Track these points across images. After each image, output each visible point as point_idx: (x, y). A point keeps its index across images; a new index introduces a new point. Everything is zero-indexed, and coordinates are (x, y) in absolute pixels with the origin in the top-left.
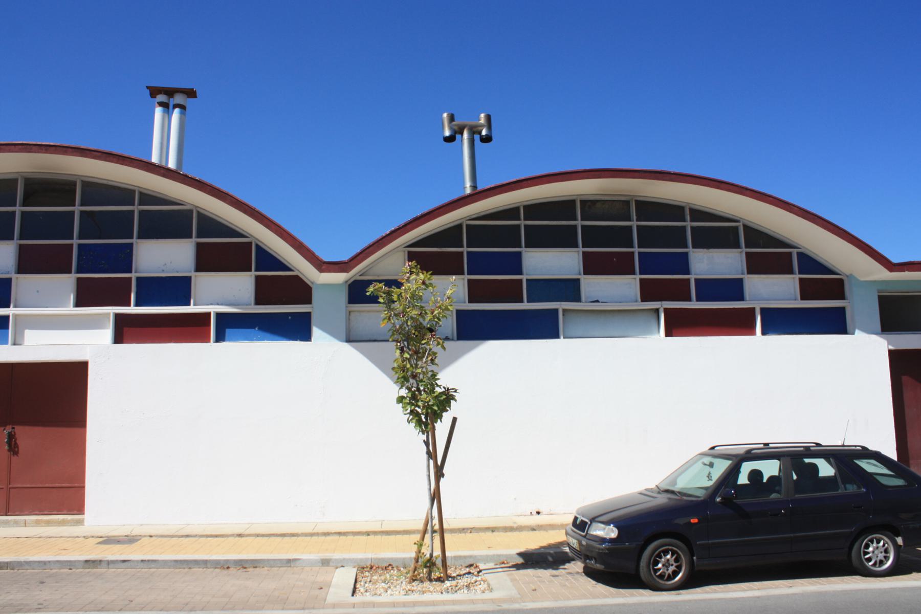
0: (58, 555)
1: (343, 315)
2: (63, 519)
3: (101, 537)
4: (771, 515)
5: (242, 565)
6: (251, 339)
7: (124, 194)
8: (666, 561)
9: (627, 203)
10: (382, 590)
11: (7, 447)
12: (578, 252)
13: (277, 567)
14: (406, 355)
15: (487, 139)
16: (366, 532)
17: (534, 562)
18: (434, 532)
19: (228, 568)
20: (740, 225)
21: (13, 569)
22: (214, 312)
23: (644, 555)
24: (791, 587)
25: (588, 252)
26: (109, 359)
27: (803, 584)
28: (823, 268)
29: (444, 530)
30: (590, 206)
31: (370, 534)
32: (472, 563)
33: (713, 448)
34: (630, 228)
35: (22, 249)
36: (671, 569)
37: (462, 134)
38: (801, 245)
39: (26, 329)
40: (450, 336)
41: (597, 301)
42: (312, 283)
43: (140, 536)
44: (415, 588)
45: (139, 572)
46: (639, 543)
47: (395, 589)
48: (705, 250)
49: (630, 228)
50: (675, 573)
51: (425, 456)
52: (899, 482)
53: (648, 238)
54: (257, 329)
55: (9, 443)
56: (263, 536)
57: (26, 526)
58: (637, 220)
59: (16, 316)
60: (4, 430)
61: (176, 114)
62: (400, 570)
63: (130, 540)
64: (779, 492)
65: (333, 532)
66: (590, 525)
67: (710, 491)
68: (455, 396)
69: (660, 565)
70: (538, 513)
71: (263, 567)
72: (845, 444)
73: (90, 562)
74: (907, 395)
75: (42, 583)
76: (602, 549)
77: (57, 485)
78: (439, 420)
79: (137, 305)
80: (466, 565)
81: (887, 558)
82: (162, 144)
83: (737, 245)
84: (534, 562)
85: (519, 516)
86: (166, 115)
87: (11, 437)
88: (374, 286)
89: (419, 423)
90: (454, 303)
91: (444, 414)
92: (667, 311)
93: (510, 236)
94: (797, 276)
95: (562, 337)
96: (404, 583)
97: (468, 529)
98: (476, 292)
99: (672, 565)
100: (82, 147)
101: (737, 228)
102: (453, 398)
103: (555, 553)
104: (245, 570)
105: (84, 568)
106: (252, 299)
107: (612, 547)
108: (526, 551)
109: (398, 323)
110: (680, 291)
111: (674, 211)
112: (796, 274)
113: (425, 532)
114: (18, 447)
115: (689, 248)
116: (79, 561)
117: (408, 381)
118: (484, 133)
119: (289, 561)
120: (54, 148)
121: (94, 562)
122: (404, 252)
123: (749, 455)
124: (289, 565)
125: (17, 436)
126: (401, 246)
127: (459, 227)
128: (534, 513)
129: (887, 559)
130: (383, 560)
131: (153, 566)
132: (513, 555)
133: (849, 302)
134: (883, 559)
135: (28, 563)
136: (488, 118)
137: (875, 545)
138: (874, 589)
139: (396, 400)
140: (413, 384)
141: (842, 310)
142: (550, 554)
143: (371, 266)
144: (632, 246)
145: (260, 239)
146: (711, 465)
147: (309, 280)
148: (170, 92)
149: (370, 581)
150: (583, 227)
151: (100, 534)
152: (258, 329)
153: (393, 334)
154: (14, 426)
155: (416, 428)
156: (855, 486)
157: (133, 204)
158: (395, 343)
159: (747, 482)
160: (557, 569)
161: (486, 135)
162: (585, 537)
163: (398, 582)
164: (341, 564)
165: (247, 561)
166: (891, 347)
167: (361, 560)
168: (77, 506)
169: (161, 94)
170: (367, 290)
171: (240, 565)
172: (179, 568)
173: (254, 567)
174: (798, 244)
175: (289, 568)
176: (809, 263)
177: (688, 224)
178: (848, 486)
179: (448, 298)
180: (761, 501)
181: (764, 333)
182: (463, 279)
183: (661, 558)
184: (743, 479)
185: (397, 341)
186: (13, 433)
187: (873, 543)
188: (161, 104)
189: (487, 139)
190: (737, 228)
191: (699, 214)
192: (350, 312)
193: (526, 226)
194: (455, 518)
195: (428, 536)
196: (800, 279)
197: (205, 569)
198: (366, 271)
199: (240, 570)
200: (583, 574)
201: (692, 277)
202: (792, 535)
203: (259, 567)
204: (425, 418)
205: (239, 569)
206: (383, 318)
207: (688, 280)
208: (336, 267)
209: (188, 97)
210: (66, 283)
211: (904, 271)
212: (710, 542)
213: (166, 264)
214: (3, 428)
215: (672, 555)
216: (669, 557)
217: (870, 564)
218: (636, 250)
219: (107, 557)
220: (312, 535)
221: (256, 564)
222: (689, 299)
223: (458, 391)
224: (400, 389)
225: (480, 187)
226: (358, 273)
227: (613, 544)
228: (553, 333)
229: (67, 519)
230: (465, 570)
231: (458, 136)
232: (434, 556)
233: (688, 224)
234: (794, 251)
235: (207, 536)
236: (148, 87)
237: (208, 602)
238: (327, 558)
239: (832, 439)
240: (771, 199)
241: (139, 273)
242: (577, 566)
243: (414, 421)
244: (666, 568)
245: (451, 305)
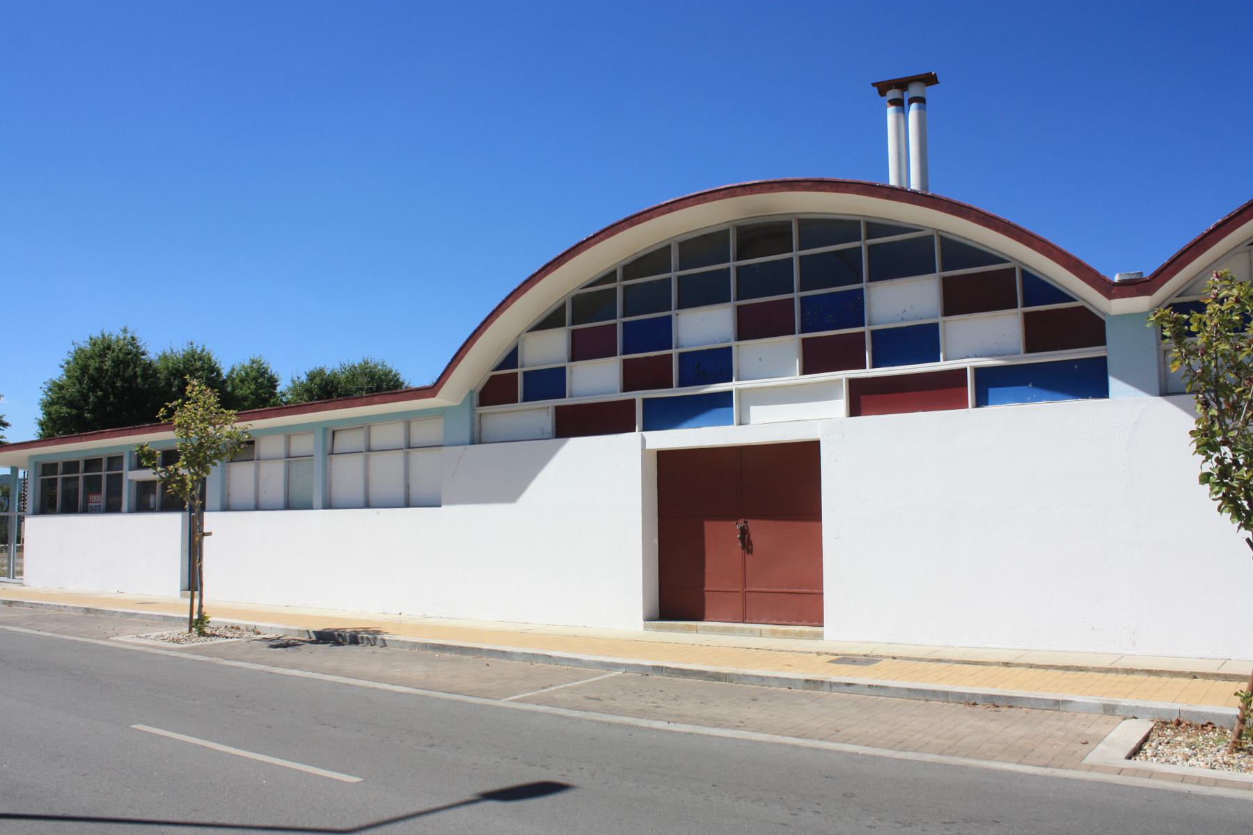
0: (779, 670)
2: (801, 631)
3: (837, 655)
5: (994, 702)
6: (1022, 400)
7: (846, 228)
10: (1180, 758)
11: (740, 544)
13: (1040, 709)
14: (1214, 412)
16: (1191, 673)
19: (975, 704)
21: (732, 682)
22: (971, 367)
26: (843, 436)
31: (1198, 677)
35: (947, 284)
42: (1104, 315)
43: (881, 656)
44: (1235, 761)
45: (864, 699)
47: (1203, 759)
54: (1030, 385)
55: (742, 539)
56: (1038, 667)
59: (740, 391)
61: (913, 111)
62: (1225, 733)
63: (868, 660)
65: (1139, 669)
71: (1021, 708)
73: (811, 682)
75: (754, 700)
77: (795, 590)
79: (874, 365)
82: (899, 154)
86: (901, 116)
87: (744, 532)
96: (1222, 752)
100: (790, 178)
104: (996, 709)
105: (804, 688)
106: (1021, 347)
109: (1196, 364)
114: (751, 544)
116: (799, 680)
119: (1057, 702)
120: (758, 187)
121: (815, 682)
124: (1057, 708)
125: (750, 531)
126: (1243, 243)
130: (1198, 714)
131: (882, 693)
135: (747, 677)
143: (1194, 280)
145: (1026, 262)
147: (1099, 311)
148: (902, 84)
149: (1168, 743)
151: (835, 651)
152: (1032, 385)
153: (1192, 382)
155: (1233, 520)
157: (859, 239)
163: (1214, 749)
164: (1133, 714)
165: (999, 697)
167: (1163, 710)
168: (816, 618)
169: (891, 88)
171: (990, 702)
172: (914, 699)
173: (1009, 707)
175: (1057, 712)
186: (746, 528)
188: (893, 102)
197: (945, 703)
198: (1190, 287)
199: (989, 709)
203: (1017, 707)
205: (989, 707)
206: (1173, 359)
208: (1132, 288)
209: (927, 86)
210: (788, 347)
213: (905, 311)
219: (830, 678)
220: (1108, 671)
221: (1010, 702)
224: (1204, 461)
226: (1173, 294)
229: (805, 631)
235: (964, 662)
236: (874, 85)
237: (927, 744)
238: (1112, 703)
241: (682, 346)
243: (1227, 509)
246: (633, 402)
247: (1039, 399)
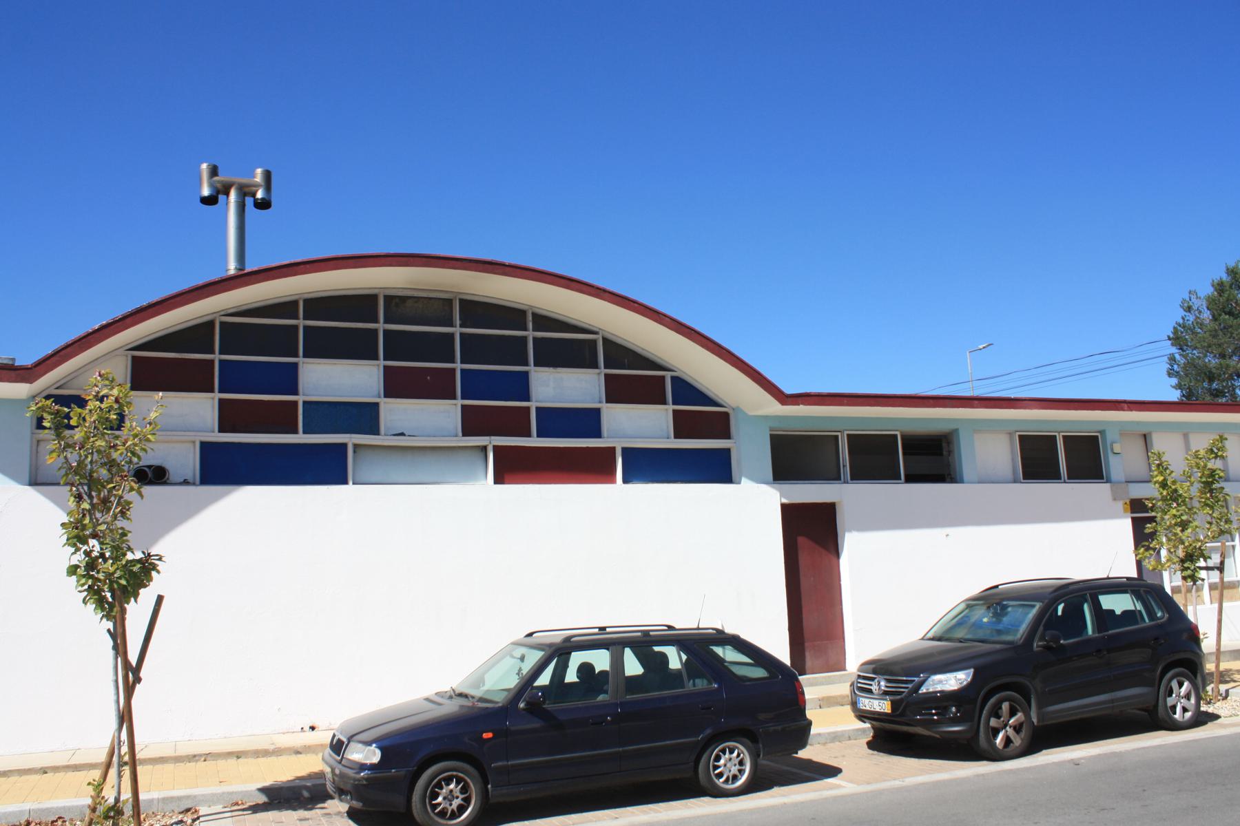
1: (25, 447)
4: (592, 724)
8: (448, 791)
9: (449, 302)
12: (378, 365)
15: (264, 205)
16: (41, 769)
17: (282, 801)
18: (122, 764)
20: (599, 338)
23: (417, 784)
24: (617, 818)
27: (645, 811)
28: (700, 397)
29: (137, 763)
30: (398, 304)
32: (190, 807)
33: (530, 635)
34: (452, 336)
36: (456, 803)
37: (227, 194)
38: (675, 367)
40: (190, 479)
41: (402, 434)
46: (411, 769)
48: (551, 369)
49: (451, 337)
50: (462, 809)
51: (111, 653)
52: (759, 673)
53: (473, 350)
58: (461, 326)
64: (606, 692)
66: (347, 746)
67: (512, 694)
68: (158, 566)
69: (440, 799)
70: (313, 728)
72: (700, 627)
74: (803, 559)
76: (359, 780)
78: (132, 599)
80: (181, 810)
81: (741, 772)
83: (594, 365)
84: (282, 801)
85: (284, 733)
88: (37, 404)
89: (101, 602)
90: (158, 430)
91: (142, 591)
92: (497, 449)
93: (283, 341)
94: (670, 408)
95: (351, 483)
97: (201, 755)
98: (230, 418)
99: (457, 797)
101: (594, 342)
102: (154, 567)
103: (314, 786)
107: (372, 775)
108: (272, 785)
110: (516, 423)
111: (512, 315)
112: (669, 405)
113: (108, 765)
115: (530, 366)
117: (85, 542)
118: (260, 195)
122: (127, 356)
123: (568, 644)
127: (210, 324)
128: (307, 728)
129: (742, 773)
132: (252, 791)
133: (735, 443)
134: (737, 773)
136: (268, 176)
137: (727, 756)
138: (720, 813)
139: (66, 571)
140: (93, 547)
141: (726, 452)
142: (306, 788)
144: (453, 361)
146: (522, 659)
150: (386, 332)
153: (67, 475)
156: (705, 682)
158: (68, 488)
159: (576, 680)
160: (311, 809)
161: (262, 199)
162: (340, 762)
166: (785, 501)
170: (72, 406)
174: (673, 366)
176: (686, 391)
177: (530, 334)
178: (698, 681)
179: (150, 424)
180: (580, 705)
181: (626, 480)
182: (213, 398)
183: (441, 788)
184: (571, 676)
185: (72, 485)
187: (725, 754)
189: (264, 205)
190: (594, 342)
191: (544, 321)
192: (38, 441)
193: (306, 328)
194: (189, 740)
195: (113, 772)
196: (674, 411)
198: (64, 384)
200: (346, 815)
201: (533, 405)
202: (621, 749)
204: (111, 596)
207: (528, 409)
211: (799, 405)
212: (509, 763)
215: (458, 783)
216: (452, 786)
217: (722, 780)
218: (458, 366)
219: (330, 755)
222: (528, 434)
223: (163, 559)
225: (248, 269)
227: (373, 772)
230: (177, 817)
231: (221, 197)
232: (121, 800)
233: (530, 334)
234: (668, 375)
239: (686, 620)
240: (636, 305)
242: (338, 806)
244: (448, 803)
245: (154, 434)
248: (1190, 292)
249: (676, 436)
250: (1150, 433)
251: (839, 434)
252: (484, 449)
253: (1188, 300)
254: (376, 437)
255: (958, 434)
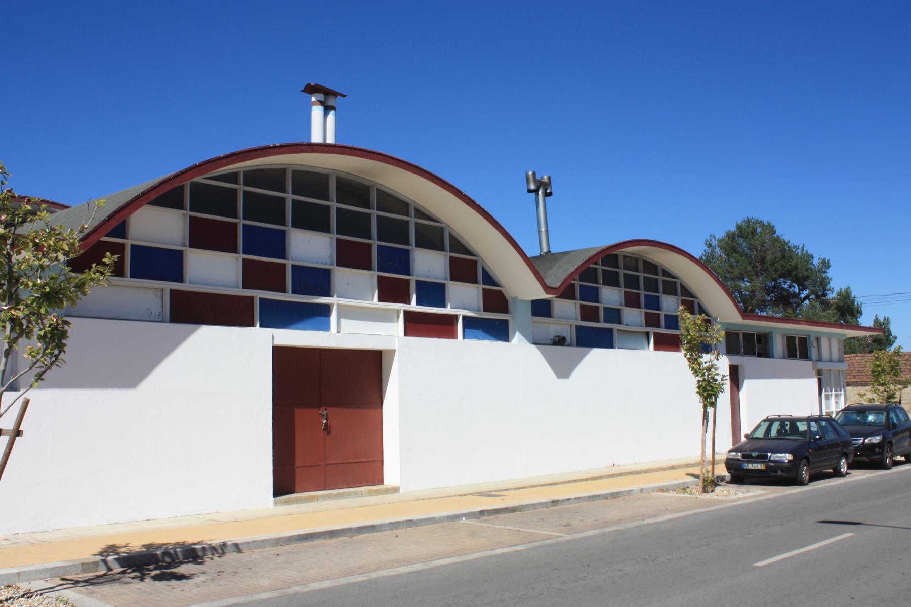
9: (637, 259)
25: (685, 300)
39: (342, 318)
56: (582, 480)
57: (363, 496)
60: (319, 410)
141: (506, 322)
154: (326, 408)
201: (289, 263)
210: (368, 278)
214: (318, 410)
218: (241, 222)
228: (610, 345)
229: (302, 496)
246: (251, 299)
247: (483, 339)
248: (711, 236)
249: (244, 287)
250: (820, 338)
251: (740, 332)
252: (647, 334)
253: (710, 240)
254: (122, 278)
255: (772, 337)
